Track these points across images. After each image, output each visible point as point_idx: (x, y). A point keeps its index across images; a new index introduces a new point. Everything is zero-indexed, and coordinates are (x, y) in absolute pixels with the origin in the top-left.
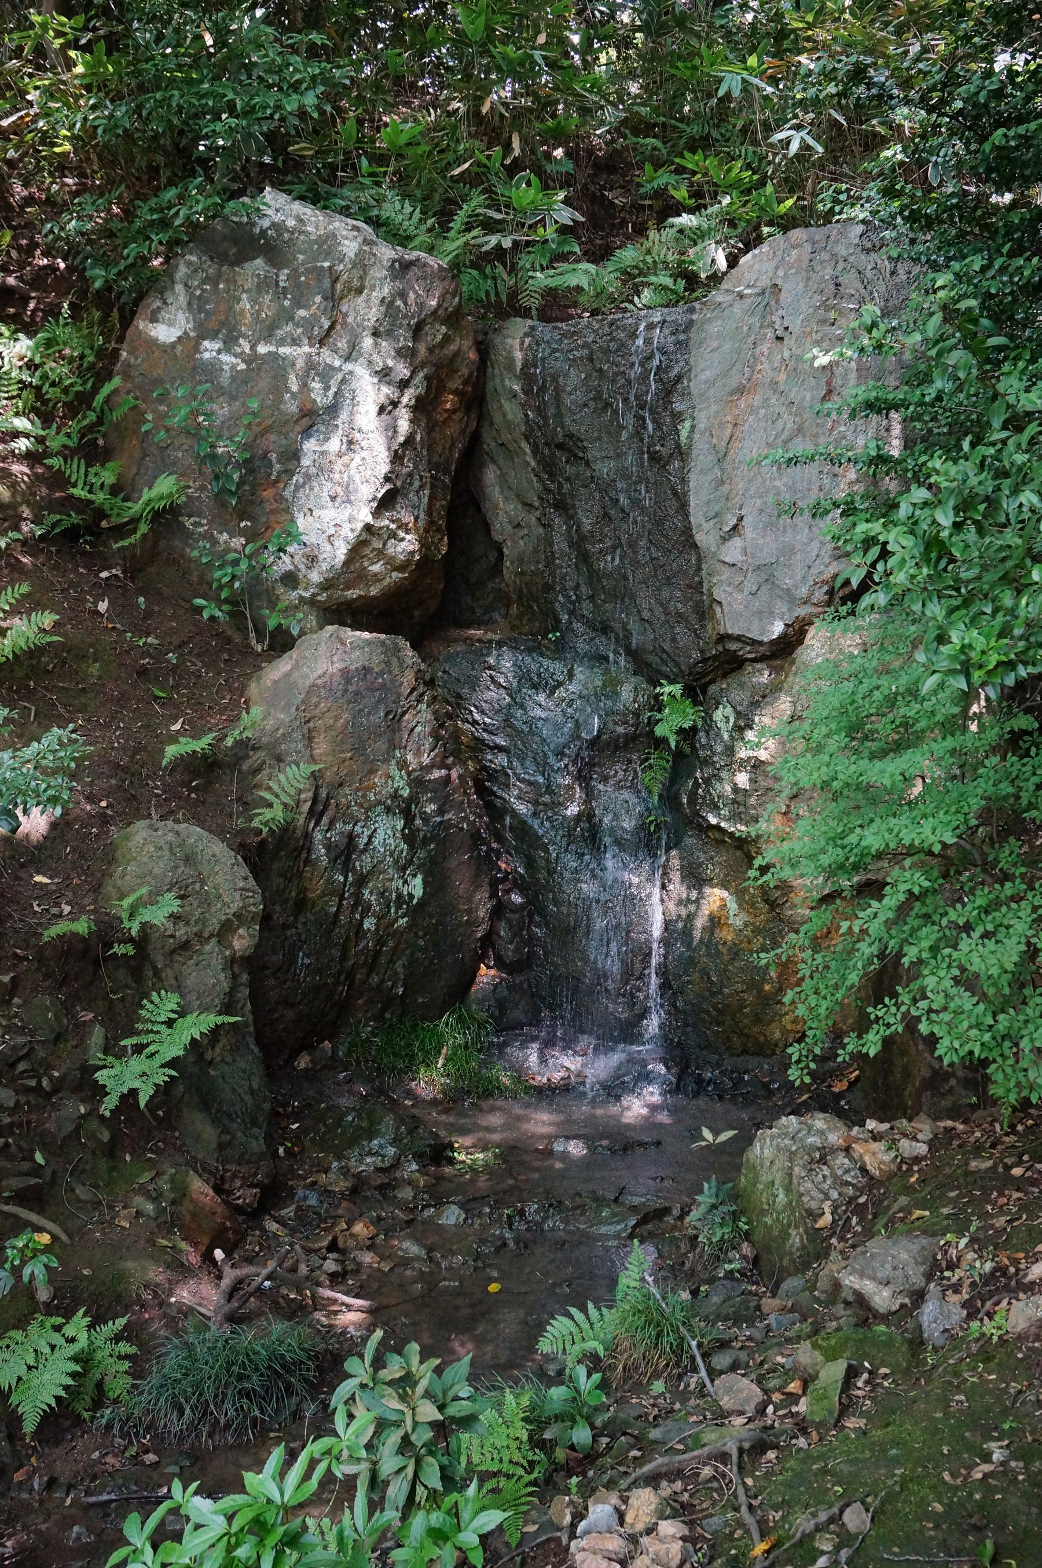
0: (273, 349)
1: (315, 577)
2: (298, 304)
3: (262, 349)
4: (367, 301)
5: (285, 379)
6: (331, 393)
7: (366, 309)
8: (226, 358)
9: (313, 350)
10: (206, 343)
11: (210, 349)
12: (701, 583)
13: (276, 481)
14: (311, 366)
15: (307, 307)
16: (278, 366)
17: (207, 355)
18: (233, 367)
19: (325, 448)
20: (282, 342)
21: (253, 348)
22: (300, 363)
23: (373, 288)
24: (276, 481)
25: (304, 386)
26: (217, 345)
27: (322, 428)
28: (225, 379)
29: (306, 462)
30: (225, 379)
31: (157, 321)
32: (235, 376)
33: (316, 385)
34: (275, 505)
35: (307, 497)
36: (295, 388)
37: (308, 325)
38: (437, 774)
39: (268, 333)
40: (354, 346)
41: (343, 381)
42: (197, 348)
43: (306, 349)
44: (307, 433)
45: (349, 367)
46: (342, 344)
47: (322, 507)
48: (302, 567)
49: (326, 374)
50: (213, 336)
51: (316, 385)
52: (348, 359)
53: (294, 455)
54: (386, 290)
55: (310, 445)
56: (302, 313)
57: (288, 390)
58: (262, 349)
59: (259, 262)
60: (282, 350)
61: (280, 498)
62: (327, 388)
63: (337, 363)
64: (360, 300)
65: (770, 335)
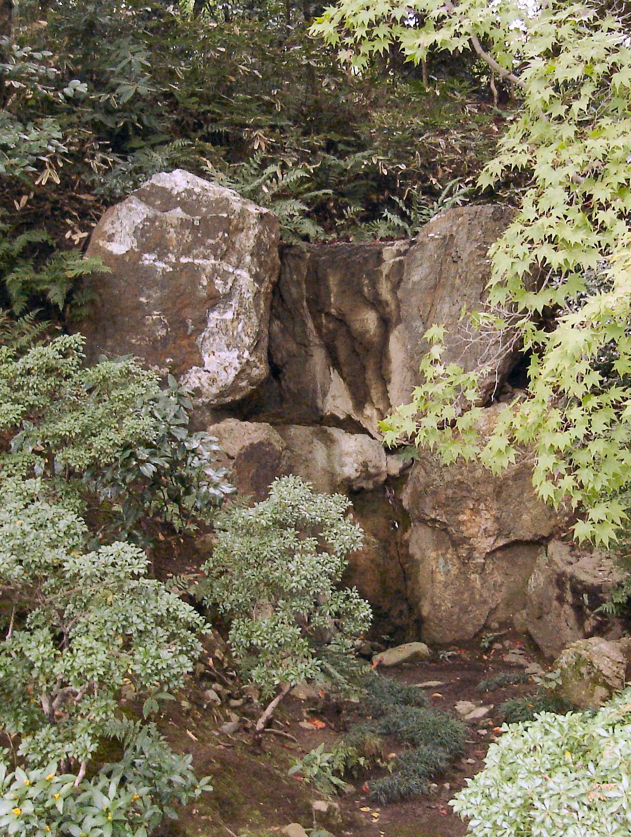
0: (190, 260)
1: (214, 390)
2: (208, 235)
3: (184, 260)
4: (247, 236)
5: (200, 278)
6: (228, 287)
7: (247, 240)
8: (160, 265)
9: (217, 262)
10: (146, 256)
11: (148, 259)
12: (349, 114)
13: (191, 335)
14: (215, 270)
15: (214, 238)
16: (193, 271)
17: (147, 262)
18: (164, 270)
19: (224, 317)
20: (196, 257)
21: (177, 259)
22: (209, 270)
23: (249, 228)
24: (191, 335)
25: (211, 282)
26: (153, 257)
27: (222, 306)
28: (159, 276)
29: (211, 325)
30: (159, 276)
31: (112, 241)
32: (165, 274)
33: (218, 282)
34: (190, 350)
35: (212, 345)
36: (205, 283)
37: (214, 248)
38: (468, 101)
39: (187, 252)
40: (240, 260)
41: (235, 280)
42: (140, 258)
43: (213, 261)
44: (212, 308)
45: (238, 272)
46: (234, 259)
47: (221, 350)
48: (206, 385)
49: (224, 275)
50: (149, 251)
51: (218, 282)
52: (237, 267)
53: (204, 321)
54: (257, 230)
55: (214, 316)
56: (211, 241)
57: (200, 284)
58: (184, 260)
59: (179, 210)
60: (196, 261)
61: (192, 345)
62: (226, 284)
63: (231, 270)
64: (242, 235)
65: (449, 259)
